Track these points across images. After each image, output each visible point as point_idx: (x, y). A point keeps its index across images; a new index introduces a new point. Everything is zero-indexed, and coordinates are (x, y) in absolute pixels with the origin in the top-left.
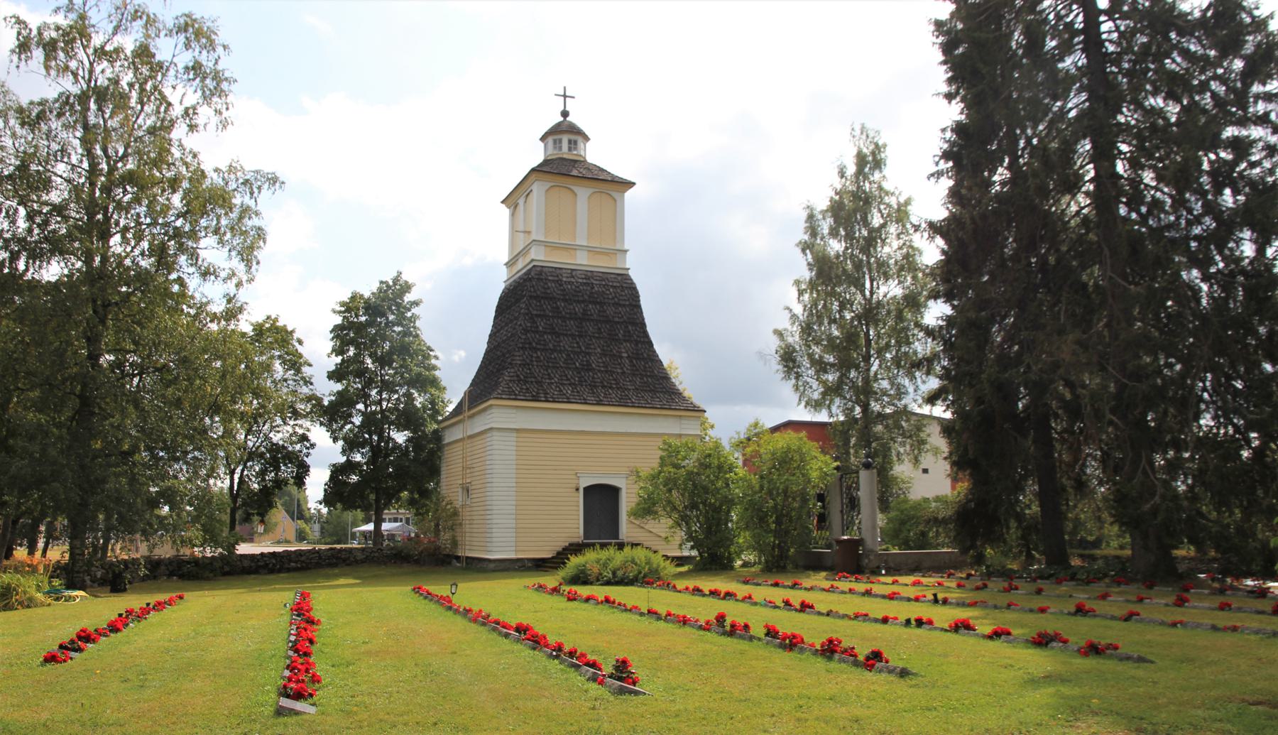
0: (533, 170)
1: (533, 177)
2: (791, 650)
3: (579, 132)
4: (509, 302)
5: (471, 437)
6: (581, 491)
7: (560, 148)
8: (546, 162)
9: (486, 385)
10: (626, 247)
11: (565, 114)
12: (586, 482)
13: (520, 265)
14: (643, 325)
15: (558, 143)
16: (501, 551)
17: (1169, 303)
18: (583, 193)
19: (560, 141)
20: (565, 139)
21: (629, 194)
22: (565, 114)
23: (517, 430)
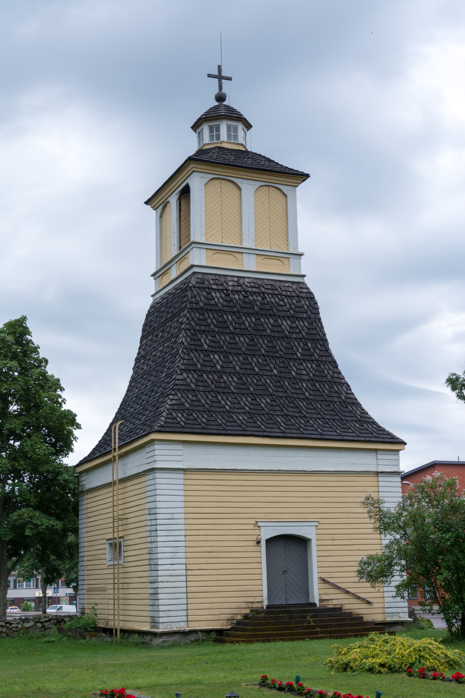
0: (190, 159)
1: (192, 166)
2: (112, 691)
3: (239, 118)
4: (161, 321)
5: (122, 481)
6: (263, 543)
7: (218, 137)
8: (200, 152)
9: (135, 422)
10: (300, 251)
11: (220, 98)
12: (267, 533)
13: (174, 273)
14: (324, 341)
15: (215, 131)
16: (172, 619)
17: (39, 491)
18: (249, 188)
19: (218, 129)
20: (224, 126)
21: (303, 188)
22: (220, 98)
23: (184, 470)
